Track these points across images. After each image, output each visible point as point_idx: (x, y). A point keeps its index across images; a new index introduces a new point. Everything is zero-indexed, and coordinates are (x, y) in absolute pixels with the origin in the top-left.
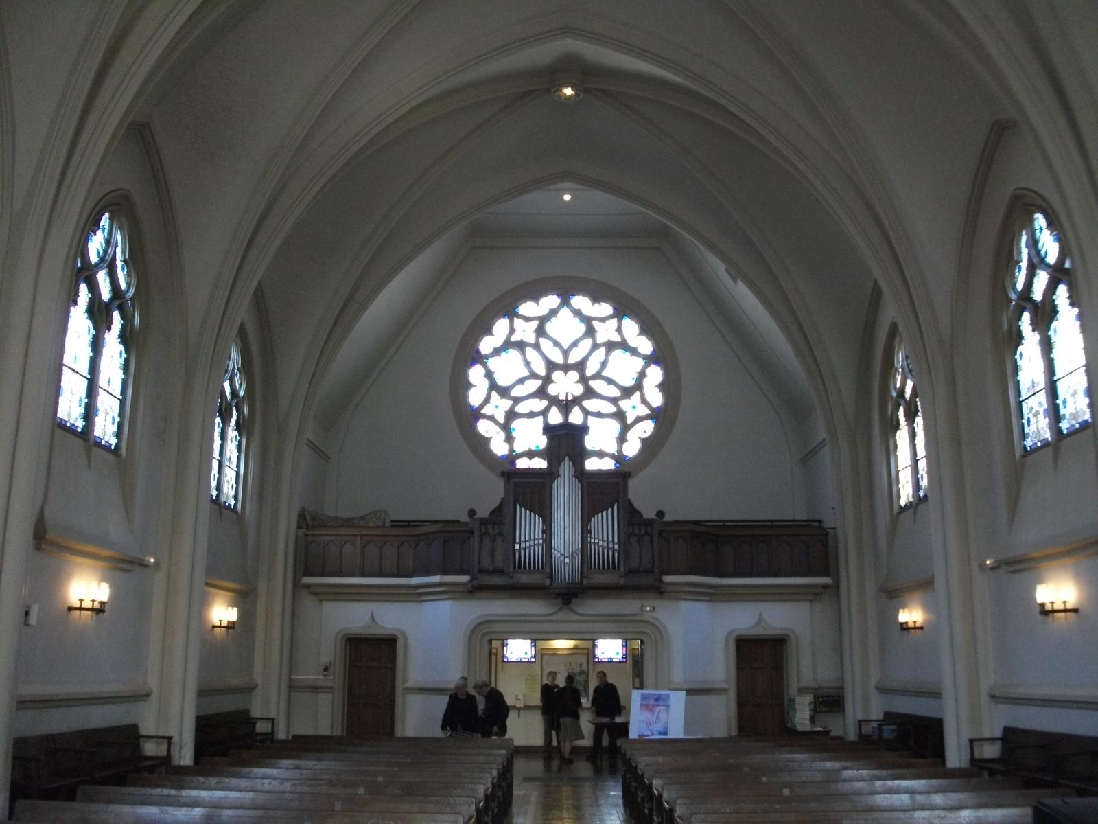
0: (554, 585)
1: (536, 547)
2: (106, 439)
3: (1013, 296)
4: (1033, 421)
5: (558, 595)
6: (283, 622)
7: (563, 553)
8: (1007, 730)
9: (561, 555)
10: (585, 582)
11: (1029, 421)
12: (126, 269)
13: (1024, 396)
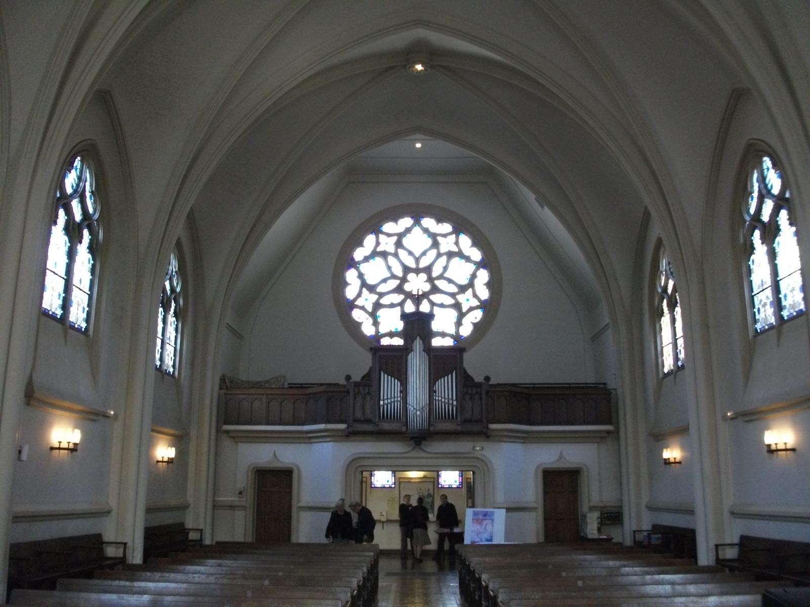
0: (409, 431)
1: (396, 403)
2: (78, 323)
3: (747, 218)
4: (762, 310)
5: (412, 438)
6: (209, 458)
7: (415, 407)
8: (743, 538)
9: (414, 409)
10: (432, 429)
11: (759, 310)
12: (93, 198)
13: (755, 292)
